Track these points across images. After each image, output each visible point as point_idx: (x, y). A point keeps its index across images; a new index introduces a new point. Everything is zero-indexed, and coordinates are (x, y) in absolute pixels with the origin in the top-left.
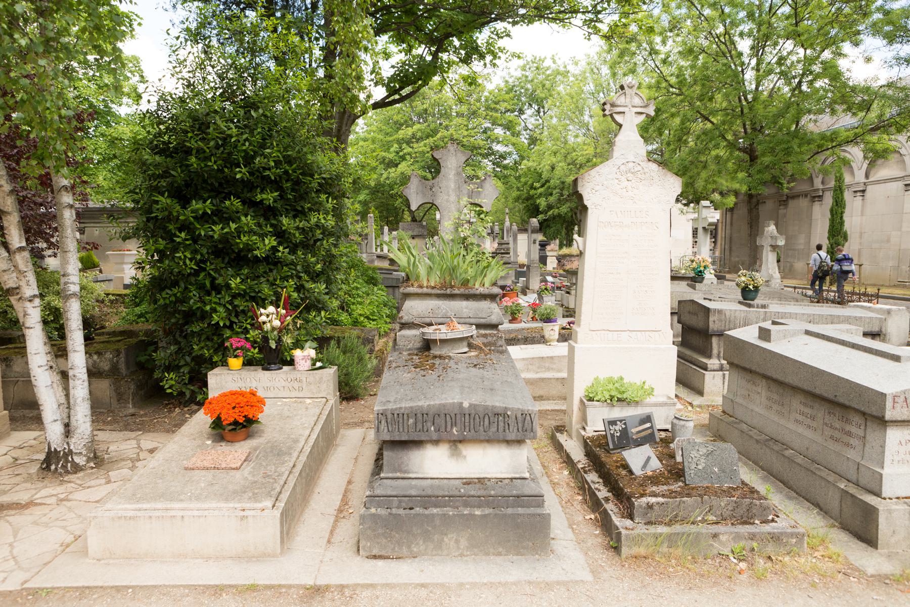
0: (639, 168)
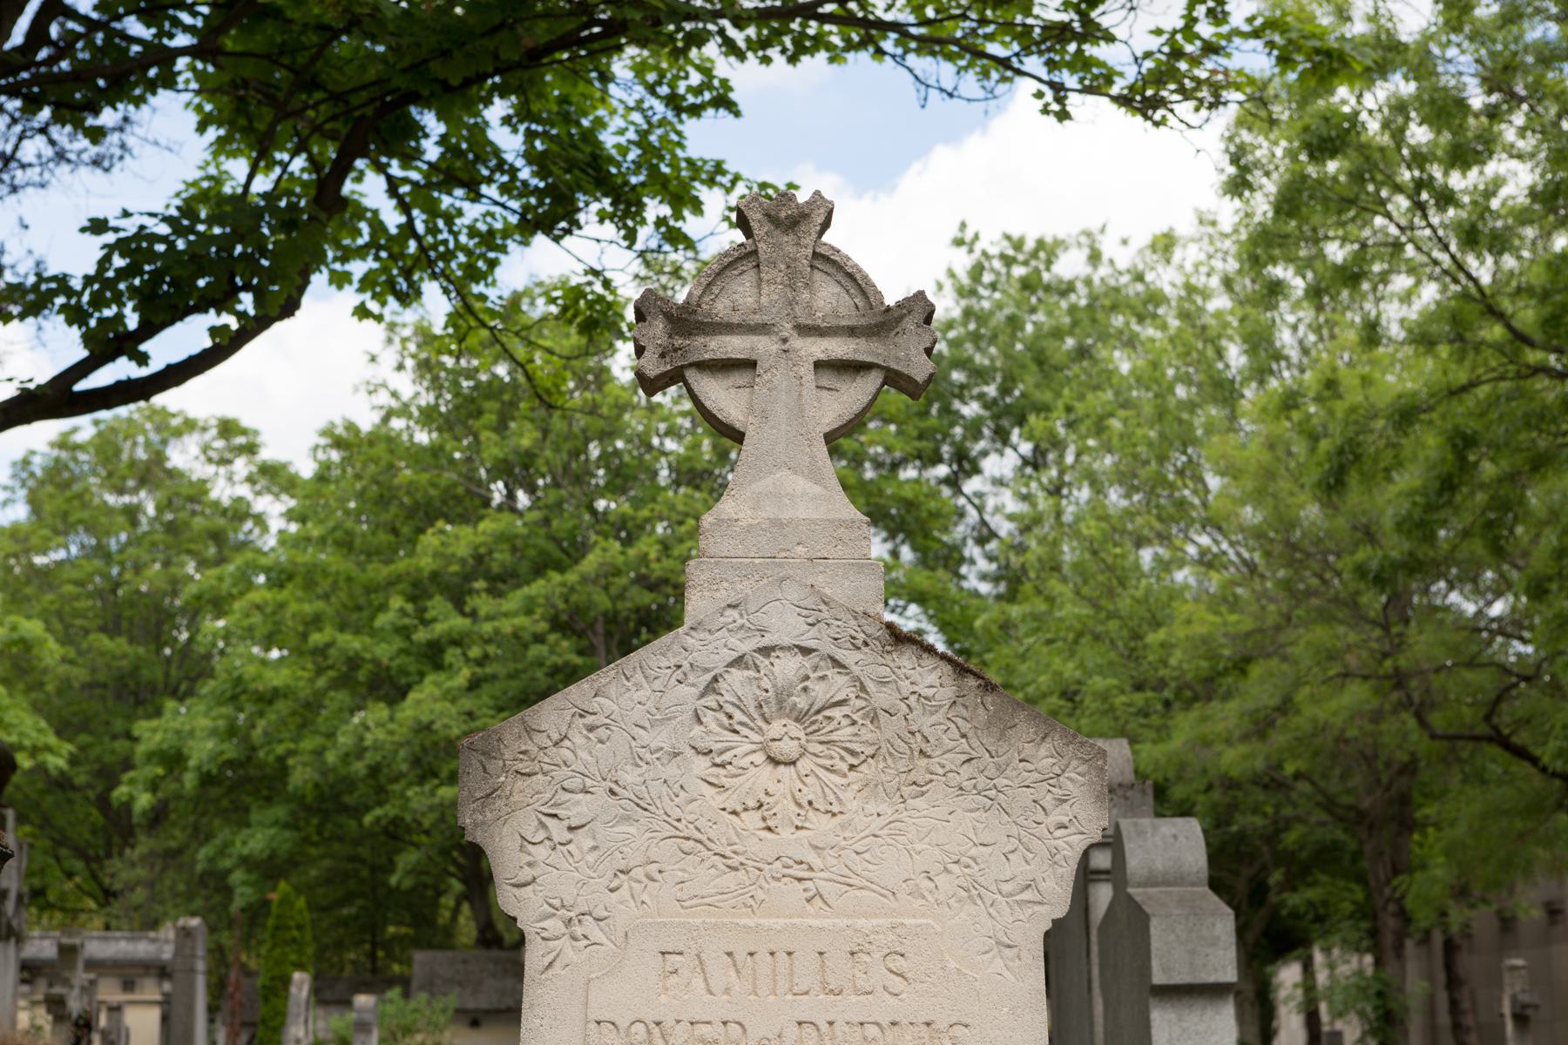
0: (839, 685)
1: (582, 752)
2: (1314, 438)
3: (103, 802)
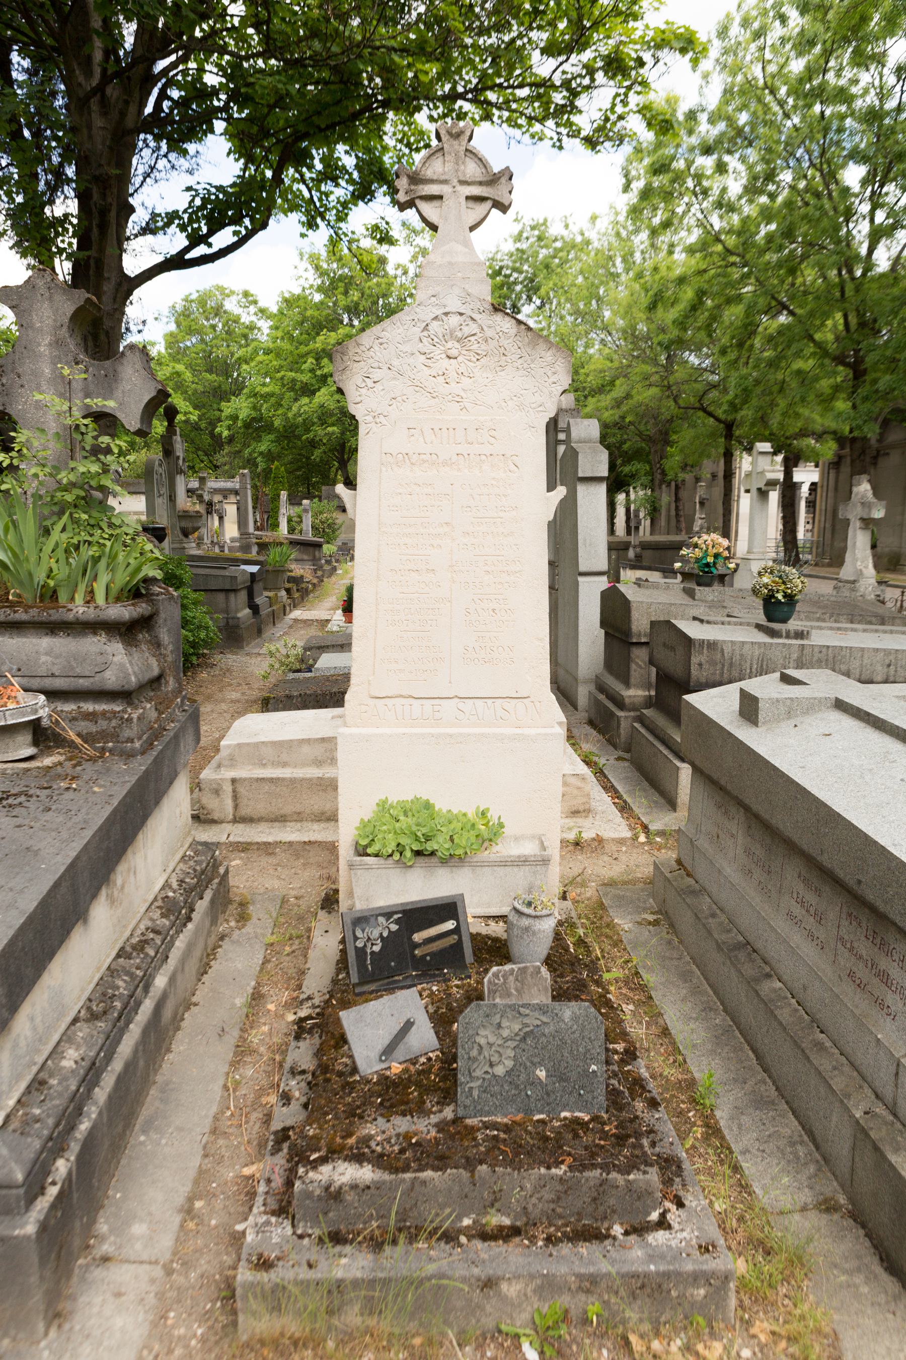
0: (473, 328)
1: (378, 353)
2: (647, 291)
3: (212, 435)
